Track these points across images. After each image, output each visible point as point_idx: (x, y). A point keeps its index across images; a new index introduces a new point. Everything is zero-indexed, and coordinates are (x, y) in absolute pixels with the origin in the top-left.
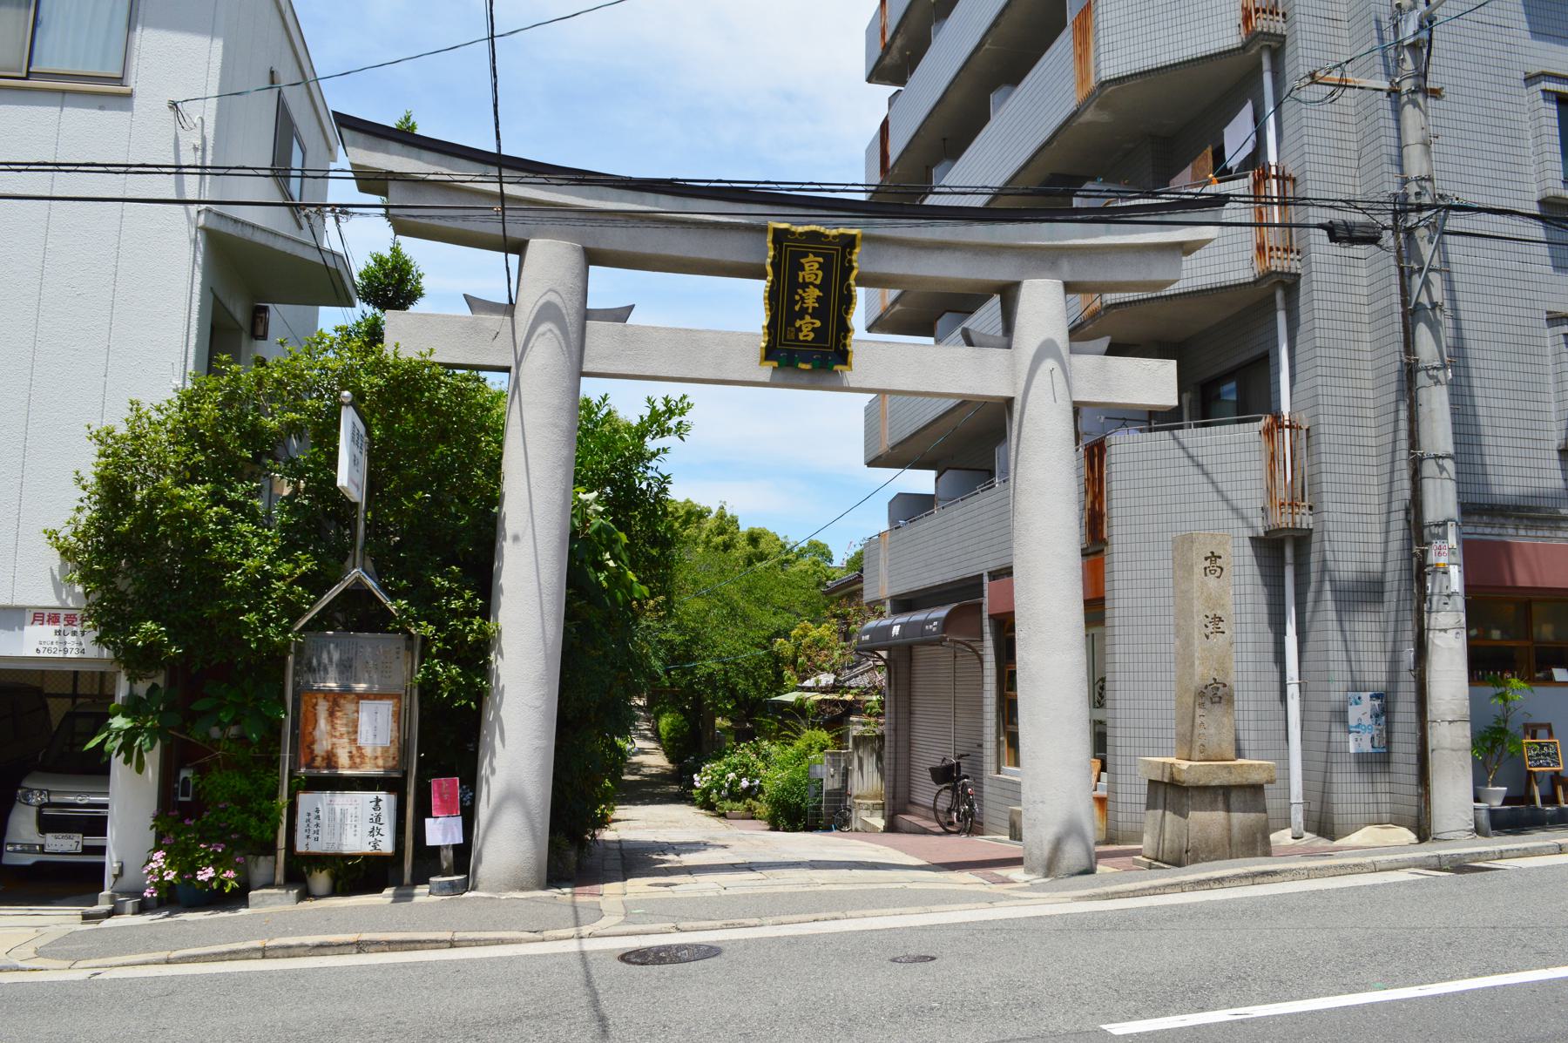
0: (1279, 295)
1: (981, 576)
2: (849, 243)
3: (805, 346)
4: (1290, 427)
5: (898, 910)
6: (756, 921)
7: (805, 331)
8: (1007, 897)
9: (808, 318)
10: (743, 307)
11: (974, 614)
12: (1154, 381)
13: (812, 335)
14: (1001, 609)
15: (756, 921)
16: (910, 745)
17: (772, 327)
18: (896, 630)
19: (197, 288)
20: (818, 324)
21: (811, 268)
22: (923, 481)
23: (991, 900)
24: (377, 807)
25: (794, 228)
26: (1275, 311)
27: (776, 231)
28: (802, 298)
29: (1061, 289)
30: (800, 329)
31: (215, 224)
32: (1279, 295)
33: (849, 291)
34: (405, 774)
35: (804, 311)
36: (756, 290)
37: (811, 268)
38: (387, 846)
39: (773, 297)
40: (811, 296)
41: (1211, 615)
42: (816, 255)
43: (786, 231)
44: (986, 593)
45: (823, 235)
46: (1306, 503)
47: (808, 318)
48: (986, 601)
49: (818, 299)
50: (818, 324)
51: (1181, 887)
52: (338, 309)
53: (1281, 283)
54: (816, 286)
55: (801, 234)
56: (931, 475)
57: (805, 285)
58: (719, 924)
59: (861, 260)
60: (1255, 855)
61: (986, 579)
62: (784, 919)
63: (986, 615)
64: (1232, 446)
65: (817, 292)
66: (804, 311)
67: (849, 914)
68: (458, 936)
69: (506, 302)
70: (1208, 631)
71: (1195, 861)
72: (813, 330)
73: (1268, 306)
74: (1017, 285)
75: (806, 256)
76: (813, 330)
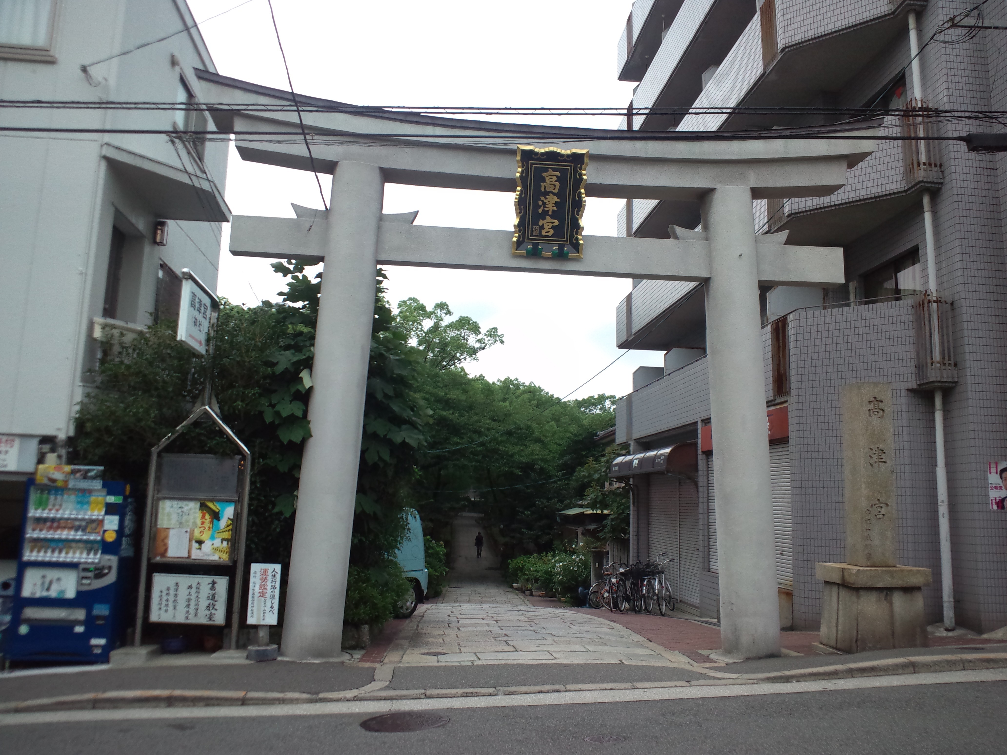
0: (926, 200)
1: (697, 422)
2: (578, 159)
3: (548, 237)
4: (937, 301)
5: (609, 686)
6: (491, 690)
7: (547, 229)
8: (703, 676)
9: (548, 219)
10: (498, 212)
11: (687, 452)
12: (825, 264)
13: (552, 232)
14: (706, 449)
15: (491, 690)
16: (648, 547)
17: (520, 226)
18: (636, 463)
19: (99, 201)
20: (556, 223)
21: (551, 180)
22: (655, 358)
23: (689, 678)
24: (213, 588)
25: (537, 150)
26: (922, 212)
27: (523, 151)
28: (544, 204)
29: (748, 194)
30: (542, 227)
31: (107, 152)
32: (926, 200)
33: (580, 198)
34: (235, 563)
35: (545, 213)
36: (508, 200)
37: (551, 180)
38: (219, 618)
39: (521, 204)
40: (551, 202)
41: (874, 447)
42: (555, 170)
43: (531, 151)
44: (700, 436)
45: (559, 154)
46: (952, 362)
47: (548, 219)
48: (700, 441)
49: (556, 204)
50: (556, 223)
51: (851, 673)
52: (207, 224)
53: (927, 190)
54: (554, 194)
55: (542, 154)
56: (660, 354)
57: (546, 194)
58: (460, 691)
59: (589, 175)
60: (915, 646)
61: (699, 425)
62: (513, 689)
63: (700, 452)
64: (886, 319)
65: (556, 199)
66: (545, 213)
67: (569, 687)
68: (252, 695)
69: (324, 209)
70: (872, 461)
71: (864, 650)
72: (553, 227)
73: (918, 209)
74: (712, 190)
75: (546, 170)
76: (553, 227)
